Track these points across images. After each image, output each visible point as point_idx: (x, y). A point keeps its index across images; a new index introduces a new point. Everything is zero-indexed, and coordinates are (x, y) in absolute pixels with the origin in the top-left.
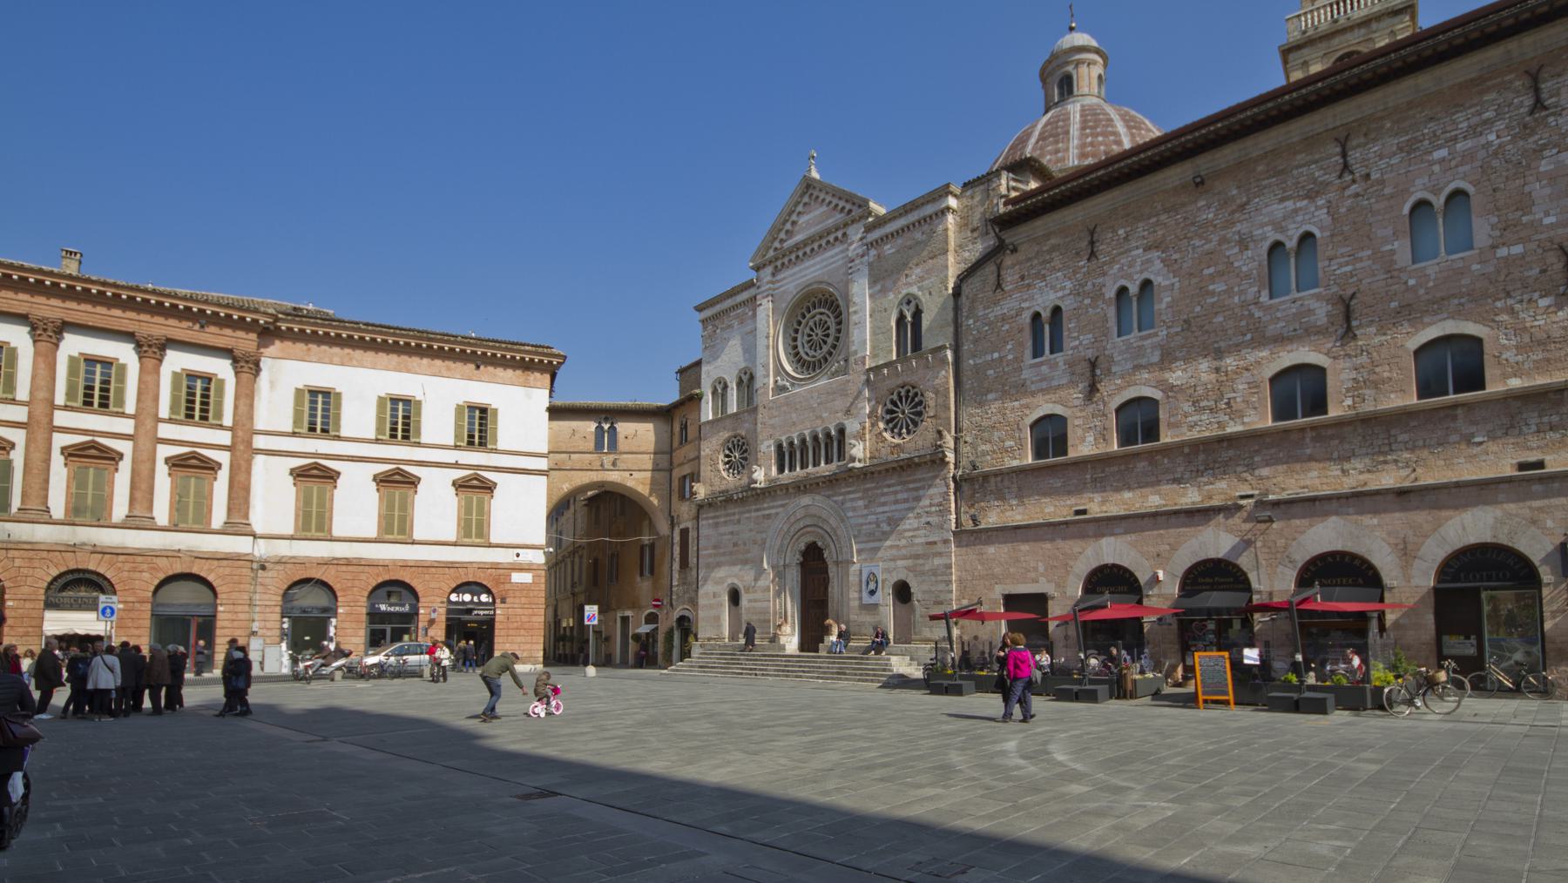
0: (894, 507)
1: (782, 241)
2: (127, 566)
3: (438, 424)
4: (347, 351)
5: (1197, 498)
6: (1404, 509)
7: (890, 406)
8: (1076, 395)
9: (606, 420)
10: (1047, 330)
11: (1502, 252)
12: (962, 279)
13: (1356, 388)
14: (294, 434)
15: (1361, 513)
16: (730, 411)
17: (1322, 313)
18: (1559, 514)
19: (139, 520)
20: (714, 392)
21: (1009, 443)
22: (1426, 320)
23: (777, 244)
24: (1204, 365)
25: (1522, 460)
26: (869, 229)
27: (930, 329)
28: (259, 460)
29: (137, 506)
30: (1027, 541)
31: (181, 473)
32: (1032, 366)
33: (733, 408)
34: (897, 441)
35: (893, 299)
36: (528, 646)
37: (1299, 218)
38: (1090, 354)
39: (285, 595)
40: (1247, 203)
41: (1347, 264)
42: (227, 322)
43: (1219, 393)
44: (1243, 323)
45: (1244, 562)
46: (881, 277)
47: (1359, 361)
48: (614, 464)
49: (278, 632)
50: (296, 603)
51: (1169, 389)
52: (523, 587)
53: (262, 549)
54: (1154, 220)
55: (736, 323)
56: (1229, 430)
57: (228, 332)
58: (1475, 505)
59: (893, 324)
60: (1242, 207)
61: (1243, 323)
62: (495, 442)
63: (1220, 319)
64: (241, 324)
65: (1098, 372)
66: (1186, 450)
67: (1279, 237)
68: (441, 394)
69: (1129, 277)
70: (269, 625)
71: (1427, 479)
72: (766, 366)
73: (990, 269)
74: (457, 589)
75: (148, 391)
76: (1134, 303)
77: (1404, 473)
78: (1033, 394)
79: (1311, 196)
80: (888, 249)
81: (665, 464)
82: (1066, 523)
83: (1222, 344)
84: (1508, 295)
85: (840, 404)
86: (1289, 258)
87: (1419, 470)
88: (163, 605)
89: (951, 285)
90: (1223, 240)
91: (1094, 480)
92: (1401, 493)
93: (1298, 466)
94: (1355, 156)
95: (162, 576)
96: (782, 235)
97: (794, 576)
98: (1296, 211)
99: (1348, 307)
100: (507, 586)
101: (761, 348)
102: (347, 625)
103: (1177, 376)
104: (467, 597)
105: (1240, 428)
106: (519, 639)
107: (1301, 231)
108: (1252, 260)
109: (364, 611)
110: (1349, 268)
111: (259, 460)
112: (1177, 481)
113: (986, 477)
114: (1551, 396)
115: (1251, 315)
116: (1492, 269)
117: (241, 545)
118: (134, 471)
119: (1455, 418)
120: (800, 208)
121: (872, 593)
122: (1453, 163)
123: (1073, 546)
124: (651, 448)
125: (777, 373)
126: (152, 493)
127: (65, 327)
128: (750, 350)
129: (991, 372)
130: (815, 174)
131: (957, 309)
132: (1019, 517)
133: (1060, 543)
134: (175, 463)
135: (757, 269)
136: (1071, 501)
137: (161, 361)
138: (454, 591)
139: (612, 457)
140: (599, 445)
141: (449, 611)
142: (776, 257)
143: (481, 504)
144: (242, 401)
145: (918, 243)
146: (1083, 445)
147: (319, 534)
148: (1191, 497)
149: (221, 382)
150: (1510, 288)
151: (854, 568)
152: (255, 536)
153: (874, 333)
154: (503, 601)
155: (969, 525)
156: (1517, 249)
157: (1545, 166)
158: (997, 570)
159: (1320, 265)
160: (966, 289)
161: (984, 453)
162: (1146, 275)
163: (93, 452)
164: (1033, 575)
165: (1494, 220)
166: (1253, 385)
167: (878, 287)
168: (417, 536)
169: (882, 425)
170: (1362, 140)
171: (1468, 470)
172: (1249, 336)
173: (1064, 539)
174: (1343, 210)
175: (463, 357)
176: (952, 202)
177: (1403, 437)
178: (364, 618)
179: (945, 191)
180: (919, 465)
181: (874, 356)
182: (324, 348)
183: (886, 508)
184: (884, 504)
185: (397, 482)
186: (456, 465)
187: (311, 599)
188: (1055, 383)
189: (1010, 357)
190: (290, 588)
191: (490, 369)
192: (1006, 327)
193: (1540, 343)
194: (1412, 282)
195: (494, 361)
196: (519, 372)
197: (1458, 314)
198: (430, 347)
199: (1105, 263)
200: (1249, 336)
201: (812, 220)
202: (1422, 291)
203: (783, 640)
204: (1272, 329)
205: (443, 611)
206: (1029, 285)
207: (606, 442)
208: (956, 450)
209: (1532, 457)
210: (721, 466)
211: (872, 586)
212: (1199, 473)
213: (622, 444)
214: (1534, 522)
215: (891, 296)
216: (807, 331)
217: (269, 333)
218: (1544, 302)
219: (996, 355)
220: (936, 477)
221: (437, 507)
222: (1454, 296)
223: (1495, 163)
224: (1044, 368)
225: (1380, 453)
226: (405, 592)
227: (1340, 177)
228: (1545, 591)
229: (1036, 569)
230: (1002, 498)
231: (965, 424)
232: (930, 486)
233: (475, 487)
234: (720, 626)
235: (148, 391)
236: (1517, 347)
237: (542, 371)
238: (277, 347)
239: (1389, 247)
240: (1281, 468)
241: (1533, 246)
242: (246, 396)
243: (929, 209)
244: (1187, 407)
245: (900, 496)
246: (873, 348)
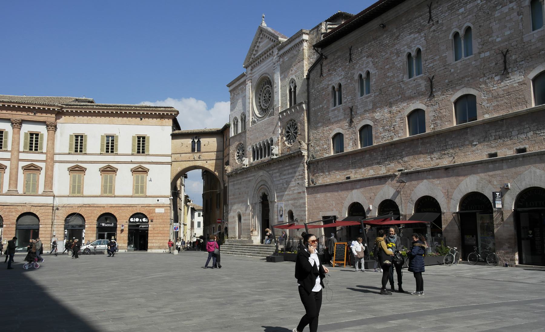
1: (254, 55)
2: (7, 210)
3: (125, 145)
4: (89, 117)
5: (385, 172)
6: (447, 177)
7: (287, 130)
8: (346, 124)
9: (196, 138)
10: (337, 92)
11: (482, 55)
12: (310, 71)
13: (435, 118)
14: (69, 154)
15: (434, 178)
16: (238, 133)
17: (423, 85)
18: (499, 178)
19: (12, 193)
20: (234, 124)
21: (325, 146)
22: (457, 88)
23: (253, 56)
24: (386, 110)
25: (518, 148)
26: (279, 50)
27: (299, 94)
28: (57, 165)
29: (11, 186)
30: (329, 192)
31: (28, 172)
32: (333, 111)
33: (240, 131)
34: (289, 146)
35: (288, 80)
36: (162, 241)
37: (415, 42)
38: (350, 105)
39: (66, 220)
40: (399, 36)
41: (431, 62)
42: (44, 111)
43: (391, 123)
44: (398, 91)
45: (397, 201)
46: (284, 71)
47: (435, 107)
48: (199, 158)
49: (63, 236)
50: (70, 223)
51: (375, 121)
52: (161, 215)
53: (58, 202)
54: (370, 44)
55: (240, 92)
56: (394, 140)
57: (44, 115)
58: (470, 174)
59: (288, 92)
60: (397, 37)
61: (398, 91)
62: (148, 151)
63: (390, 89)
64: (49, 111)
65: (353, 113)
66: (381, 149)
67: (409, 51)
68: (126, 131)
69: (361, 70)
70: (60, 232)
71: (459, 161)
72: (249, 112)
73: (319, 66)
74: (134, 216)
75: (16, 142)
76: (364, 81)
77: (451, 159)
78: (333, 123)
79: (419, 32)
80: (286, 58)
81: (222, 157)
82: (341, 183)
83: (392, 100)
84: (484, 76)
85: (271, 129)
86: (414, 60)
87: (456, 158)
88: (20, 225)
89: (306, 74)
90: (392, 53)
91: (352, 163)
92: (447, 168)
93: (416, 156)
94: (434, 12)
95: (20, 214)
96: (254, 52)
97: (259, 208)
98: (414, 39)
99: (431, 82)
100: (154, 215)
101: (247, 104)
102: (89, 232)
103: (377, 115)
104: (137, 220)
105: (397, 139)
106: (158, 238)
107: (416, 48)
108: (401, 61)
109: (96, 226)
110: (431, 65)
111: (57, 165)
112: (379, 163)
113: (318, 161)
114: (499, 122)
115: (401, 87)
116: (479, 64)
117: (48, 200)
118: (11, 173)
119: (467, 133)
120: (259, 40)
121: (281, 216)
122: (466, 14)
123: (343, 194)
124: (215, 149)
125: (253, 115)
126: (17, 181)
127: (23, 121)
128: (244, 105)
129: (319, 114)
130: (264, 25)
131: (308, 85)
132: (328, 181)
133: (341, 193)
134: (26, 169)
135: (246, 67)
136: (345, 173)
137: (20, 129)
138: (132, 217)
139: (198, 154)
140: (193, 150)
141: (129, 226)
142: (252, 62)
143: (142, 178)
144: (50, 142)
145: (295, 56)
146: (349, 148)
147: (79, 195)
148: (382, 171)
149: (7, 133)
150: (485, 72)
151: (276, 204)
152: (54, 196)
153: (282, 97)
154: (152, 221)
155: (312, 185)
156: (487, 54)
157: (497, 14)
158: (320, 205)
159: (423, 63)
160: (311, 76)
161: (317, 151)
162: (367, 69)
163: (32, 168)
164: (331, 207)
165: (480, 40)
166: (402, 119)
167: (283, 76)
168: (116, 194)
169: (285, 138)
170: (436, 5)
171: (471, 158)
172: (400, 97)
173: (341, 190)
174: (430, 38)
175: (135, 116)
176: (305, 37)
177: (450, 142)
178: (95, 229)
179: (301, 33)
180: (294, 157)
181: (282, 107)
182: (81, 117)
183: (285, 177)
184: (285, 175)
185: (109, 170)
186: (132, 162)
187: (76, 222)
188: (339, 119)
189: (325, 107)
190: (68, 217)
191: (146, 119)
192: (324, 93)
193: (496, 98)
194: (452, 70)
195: (148, 116)
196: (159, 120)
197: (468, 85)
198: (121, 113)
199: (355, 64)
200: (400, 97)
201: (264, 45)
202: (456, 75)
203: (253, 238)
204: (408, 93)
205: (127, 226)
206: (331, 74)
207: (196, 148)
208: (308, 150)
209: (493, 151)
210: (236, 158)
211: (281, 213)
212: (385, 160)
213: (203, 149)
214: (490, 182)
215: (287, 79)
216: (264, 95)
217: (59, 114)
218: (497, 78)
219: (321, 106)
220: (300, 162)
221: (124, 181)
222: (466, 76)
223: (480, 14)
224: (336, 111)
225: (444, 150)
226: (112, 218)
227: (429, 22)
228: (494, 214)
229: (332, 204)
230: (323, 172)
231: (311, 138)
232: (299, 166)
233: (140, 171)
234: (235, 232)
235: (16, 142)
236: (487, 100)
237: (169, 118)
238: (64, 118)
239: (445, 55)
240: (411, 157)
241: (493, 52)
242: (52, 140)
243: (297, 41)
244: (381, 129)
246: (282, 103)
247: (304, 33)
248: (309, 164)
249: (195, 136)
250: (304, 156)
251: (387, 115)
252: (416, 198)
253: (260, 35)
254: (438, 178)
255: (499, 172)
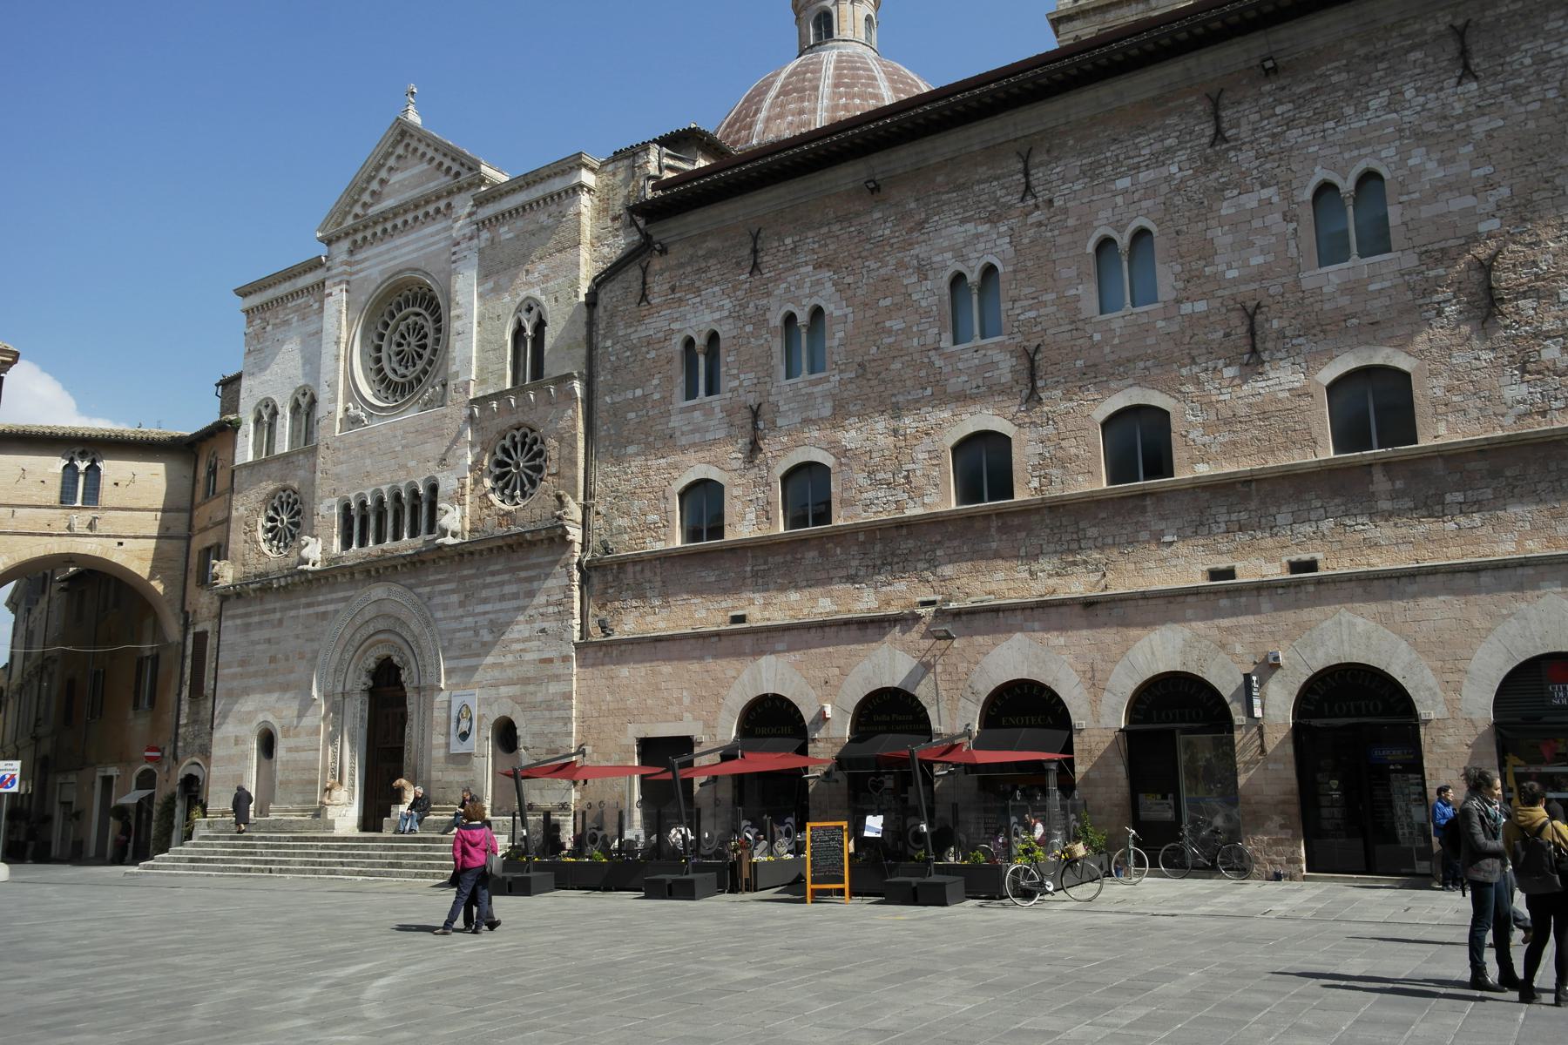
0: (498, 606)
9: (83, 456)
25: (1294, 558)
48: (91, 526)
51: (842, 453)
164: (675, 709)
183: (488, 607)
184: (485, 601)
213: (107, 494)
230: (641, 596)
231: (598, 487)
245: (508, 589)
247: (586, 166)
248: (586, 571)
249: (78, 449)
250: (572, 542)
251: (886, 441)
252: (986, 686)
253: (395, 144)
254: (1062, 628)
255: (1249, 620)
